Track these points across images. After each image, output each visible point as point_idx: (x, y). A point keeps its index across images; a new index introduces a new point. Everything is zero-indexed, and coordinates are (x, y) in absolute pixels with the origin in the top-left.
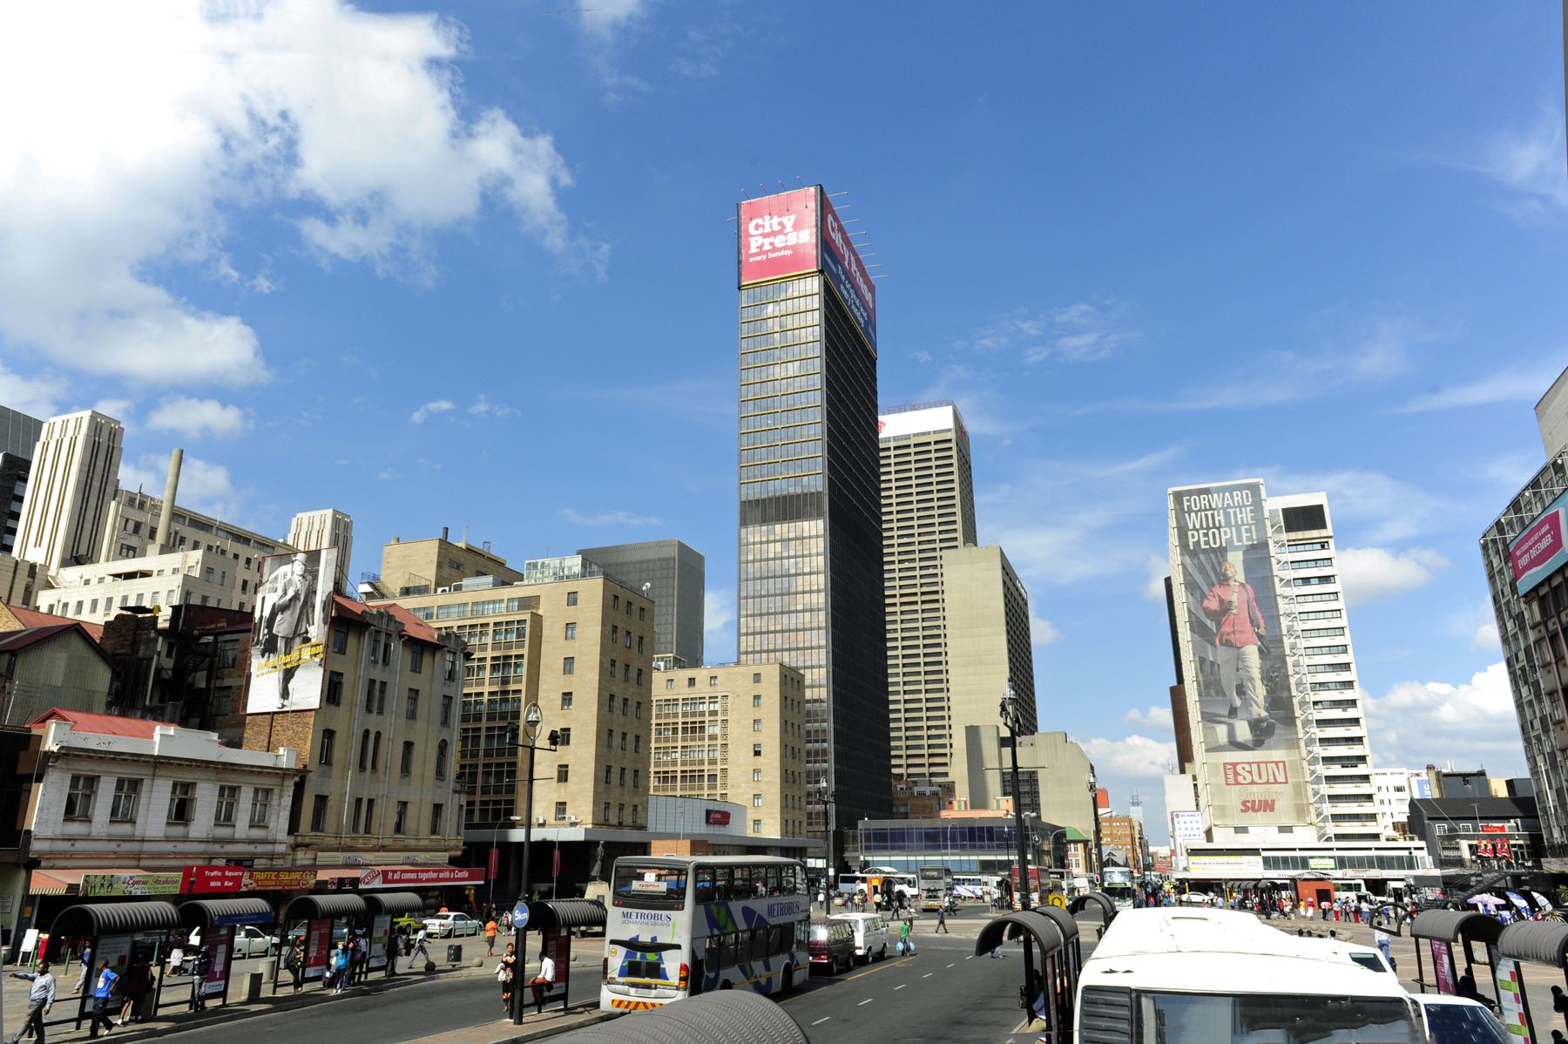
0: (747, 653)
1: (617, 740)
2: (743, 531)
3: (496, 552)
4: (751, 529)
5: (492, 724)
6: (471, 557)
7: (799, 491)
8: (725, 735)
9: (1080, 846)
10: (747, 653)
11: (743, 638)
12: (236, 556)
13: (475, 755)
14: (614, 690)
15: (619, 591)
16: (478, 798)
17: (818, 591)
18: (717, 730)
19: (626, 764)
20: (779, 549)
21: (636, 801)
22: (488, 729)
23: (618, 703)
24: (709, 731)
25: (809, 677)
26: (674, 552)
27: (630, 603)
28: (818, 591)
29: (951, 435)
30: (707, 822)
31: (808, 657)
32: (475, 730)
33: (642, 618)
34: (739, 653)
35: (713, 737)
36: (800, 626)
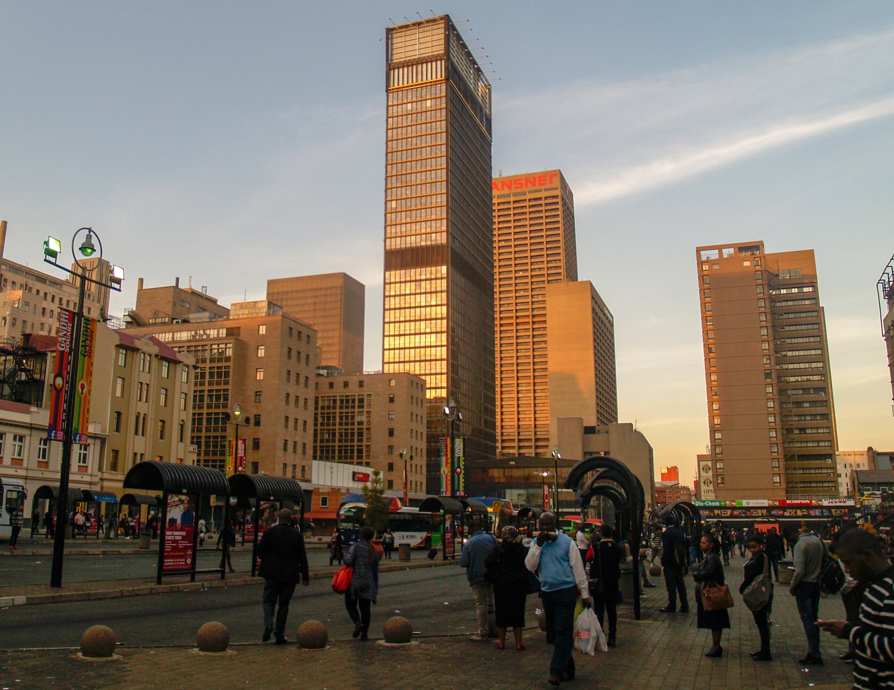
0: (389, 363)
1: (291, 424)
2: (387, 273)
3: (210, 294)
4: (393, 272)
5: (210, 411)
6: (194, 298)
7: (429, 243)
8: (369, 422)
9: (98, 442)
10: (389, 363)
11: (386, 352)
12: (38, 292)
13: (200, 431)
14: (289, 391)
15: (293, 325)
16: (205, 411)
17: (442, 319)
18: (364, 418)
19: (298, 439)
20: (413, 288)
21: (304, 463)
22: (208, 414)
23: (292, 399)
24: (358, 419)
25: (430, 381)
26: (340, 282)
27: (300, 332)
28: (442, 319)
29: (557, 192)
30: (354, 479)
31: (433, 367)
32: (200, 391)
33: (308, 343)
34: (384, 363)
35: (360, 423)
36: (428, 344)
